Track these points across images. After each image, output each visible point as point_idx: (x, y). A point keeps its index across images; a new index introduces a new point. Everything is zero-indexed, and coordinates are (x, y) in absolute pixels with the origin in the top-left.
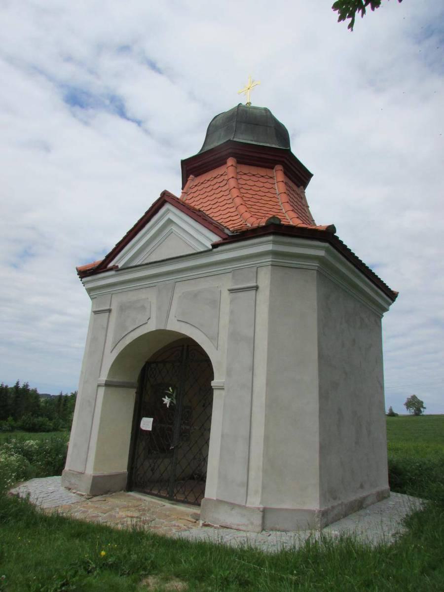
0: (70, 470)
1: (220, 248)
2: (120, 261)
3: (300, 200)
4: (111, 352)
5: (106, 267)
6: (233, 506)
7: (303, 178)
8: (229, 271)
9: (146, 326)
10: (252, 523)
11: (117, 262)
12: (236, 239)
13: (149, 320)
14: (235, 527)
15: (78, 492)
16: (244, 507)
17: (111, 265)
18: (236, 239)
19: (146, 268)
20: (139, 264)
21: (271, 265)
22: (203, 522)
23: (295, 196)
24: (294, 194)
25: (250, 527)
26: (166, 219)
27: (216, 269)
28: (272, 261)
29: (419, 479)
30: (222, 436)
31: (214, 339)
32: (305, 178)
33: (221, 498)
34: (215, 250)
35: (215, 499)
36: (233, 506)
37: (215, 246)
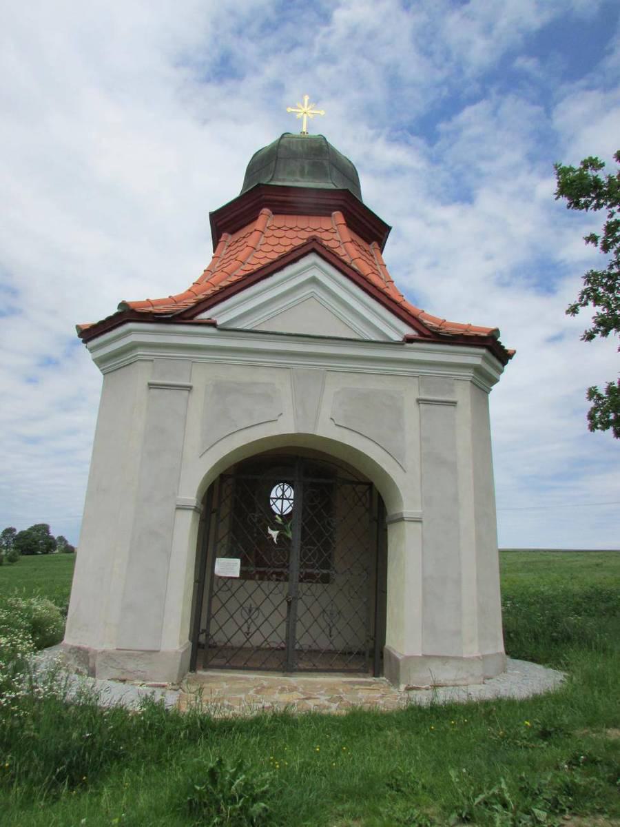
0: (117, 649)
1: (415, 345)
2: (221, 313)
3: (370, 258)
4: (405, 471)
5: (192, 317)
6: (444, 659)
7: (379, 234)
8: (417, 375)
9: (274, 424)
10: (472, 675)
11: (216, 314)
12: (440, 340)
13: (281, 417)
14: (451, 683)
15: (149, 683)
16: (460, 659)
17: (204, 316)
18: (440, 340)
19: (274, 339)
20: (248, 328)
21: (471, 381)
22: (405, 686)
23: (368, 257)
24: (367, 255)
25: (471, 680)
26: (309, 275)
27: (407, 370)
28: (473, 377)
29: (217, 693)
30: (424, 579)
31: (397, 458)
32: (381, 233)
33: (428, 653)
34: (408, 345)
35: (420, 655)
36: (444, 659)
37: (409, 340)
